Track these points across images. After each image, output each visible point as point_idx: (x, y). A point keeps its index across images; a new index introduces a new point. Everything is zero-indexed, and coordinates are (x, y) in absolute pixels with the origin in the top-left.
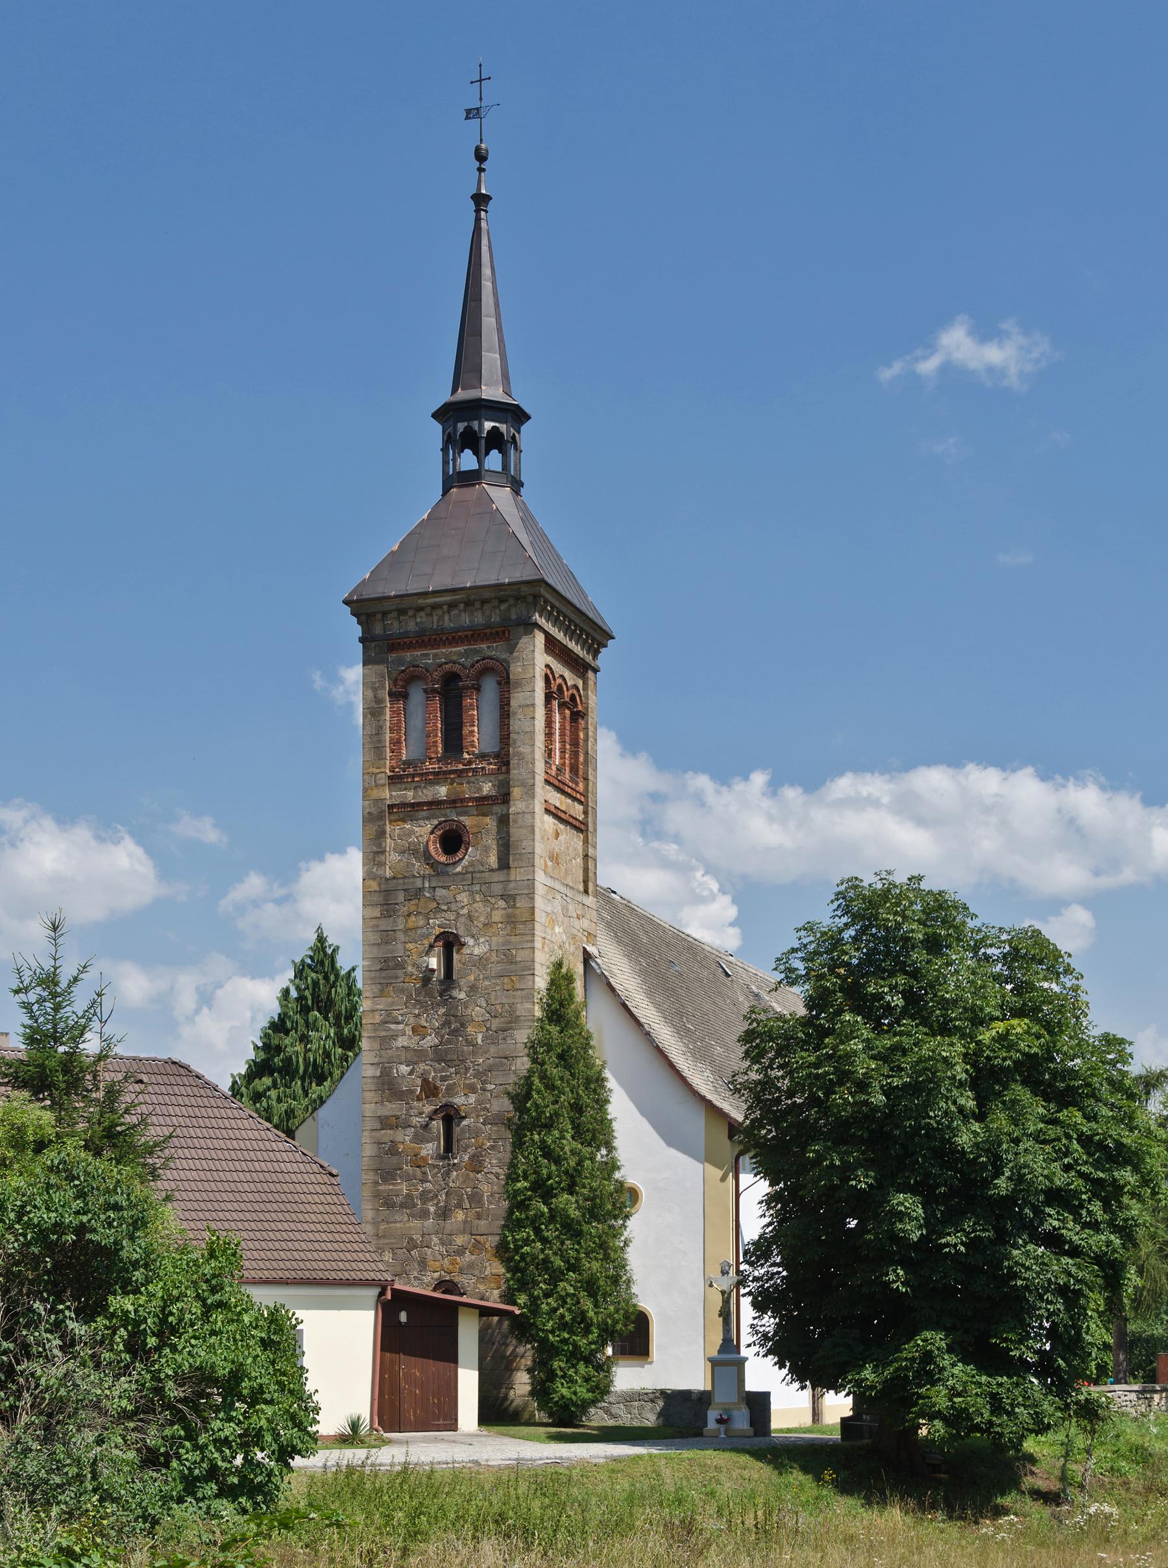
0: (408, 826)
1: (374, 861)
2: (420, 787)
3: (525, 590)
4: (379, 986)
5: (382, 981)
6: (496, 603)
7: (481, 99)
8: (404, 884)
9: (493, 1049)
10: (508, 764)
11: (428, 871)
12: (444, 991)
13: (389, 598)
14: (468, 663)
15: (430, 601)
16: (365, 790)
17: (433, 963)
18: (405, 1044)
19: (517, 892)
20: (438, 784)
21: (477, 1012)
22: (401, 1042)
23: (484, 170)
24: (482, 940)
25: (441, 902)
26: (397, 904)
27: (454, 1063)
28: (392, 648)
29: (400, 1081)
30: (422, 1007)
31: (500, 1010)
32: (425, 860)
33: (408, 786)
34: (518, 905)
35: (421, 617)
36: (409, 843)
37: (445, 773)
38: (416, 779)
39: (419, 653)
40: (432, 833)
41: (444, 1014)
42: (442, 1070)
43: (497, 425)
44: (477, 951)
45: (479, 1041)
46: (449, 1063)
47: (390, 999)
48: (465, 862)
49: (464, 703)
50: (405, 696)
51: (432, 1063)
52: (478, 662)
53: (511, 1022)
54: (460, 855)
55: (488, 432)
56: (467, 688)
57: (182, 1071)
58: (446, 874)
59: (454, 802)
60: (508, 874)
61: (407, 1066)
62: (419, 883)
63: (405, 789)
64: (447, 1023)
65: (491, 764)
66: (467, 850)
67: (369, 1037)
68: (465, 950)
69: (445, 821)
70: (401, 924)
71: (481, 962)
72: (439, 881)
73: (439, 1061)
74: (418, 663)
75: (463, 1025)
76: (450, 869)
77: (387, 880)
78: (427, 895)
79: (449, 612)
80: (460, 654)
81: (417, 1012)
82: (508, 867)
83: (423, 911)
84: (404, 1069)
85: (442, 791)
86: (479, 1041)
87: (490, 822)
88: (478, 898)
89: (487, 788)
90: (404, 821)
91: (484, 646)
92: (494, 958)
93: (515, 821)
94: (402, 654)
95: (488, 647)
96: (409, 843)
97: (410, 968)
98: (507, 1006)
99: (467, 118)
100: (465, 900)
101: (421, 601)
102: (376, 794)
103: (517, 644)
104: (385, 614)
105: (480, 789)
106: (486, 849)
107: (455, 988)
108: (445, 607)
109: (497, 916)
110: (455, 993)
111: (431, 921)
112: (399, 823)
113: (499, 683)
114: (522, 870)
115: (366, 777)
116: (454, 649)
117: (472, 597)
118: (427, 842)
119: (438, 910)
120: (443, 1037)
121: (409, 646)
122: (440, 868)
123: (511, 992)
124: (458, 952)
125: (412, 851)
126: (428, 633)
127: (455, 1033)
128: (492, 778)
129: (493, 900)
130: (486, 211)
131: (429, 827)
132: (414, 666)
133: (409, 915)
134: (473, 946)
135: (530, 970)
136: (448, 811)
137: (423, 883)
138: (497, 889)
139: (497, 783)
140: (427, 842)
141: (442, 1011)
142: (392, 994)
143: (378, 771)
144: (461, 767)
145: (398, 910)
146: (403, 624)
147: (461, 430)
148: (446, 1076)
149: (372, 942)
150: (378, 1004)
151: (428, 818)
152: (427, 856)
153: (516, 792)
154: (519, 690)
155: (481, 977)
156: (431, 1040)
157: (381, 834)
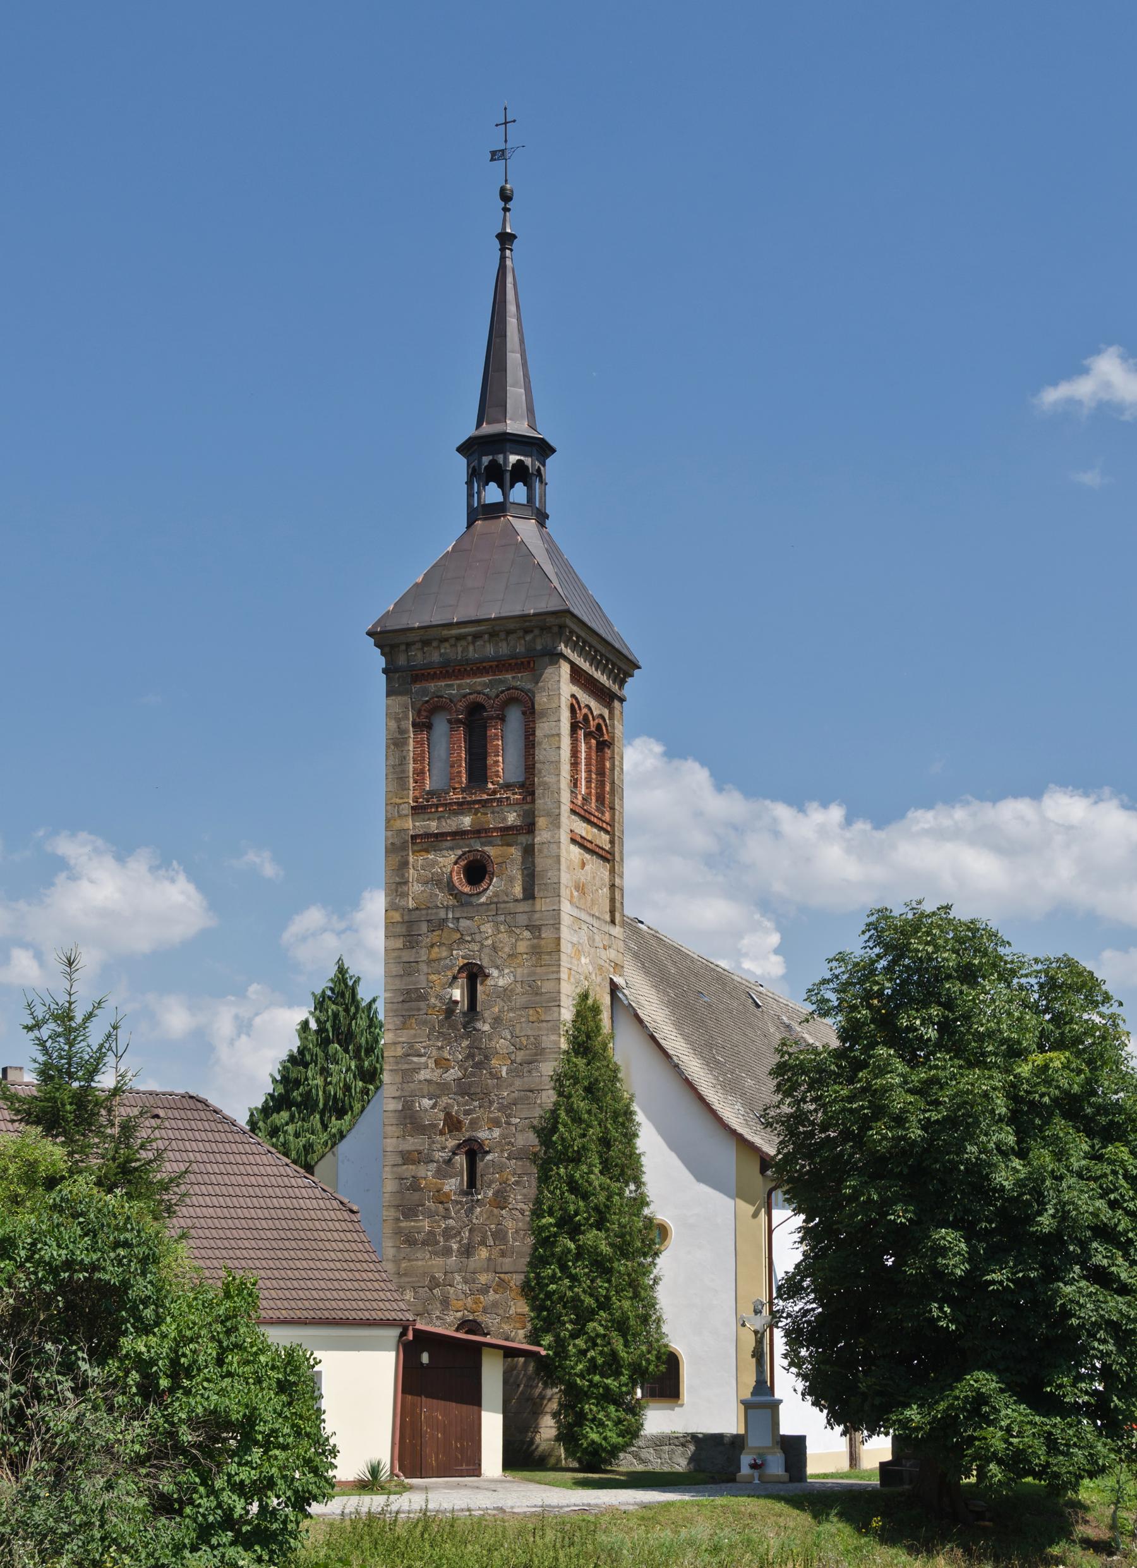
0: (431, 857)
1: (397, 892)
2: (443, 817)
3: (551, 620)
4: (401, 1019)
5: (404, 1013)
6: (521, 633)
8: (427, 915)
9: (518, 1082)
10: (533, 793)
13: (413, 629)
15: (455, 632)
16: (388, 820)
17: (457, 994)
18: (428, 1077)
19: (542, 922)
20: (462, 814)
21: (502, 1044)
22: (424, 1075)
23: (509, 210)
24: (506, 971)
25: (465, 933)
26: (420, 935)
28: (416, 679)
31: (525, 1043)
32: (449, 891)
33: (431, 816)
34: (543, 936)
35: (445, 648)
37: (469, 803)
39: (443, 684)
40: (456, 863)
41: (468, 1047)
42: (466, 1104)
43: (522, 458)
44: (501, 982)
45: (504, 1074)
46: (472, 1096)
47: (412, 1032)
48: (489, 893)
49: (489, 733)
50: (428, 727)
51: (455, 1097)
52: (502, 692)
54: (484, 885)
55: (513, 465)
56: (492, 718)
59: (478, 832)
60: (533, 904)
62: (442, 914)
63: (429, 819)
64: (470, 1056)
65: (516, 793)
66: (491, 880)
67: (391, 1070)
68: (490, 982)
69: (469, 852)
70: (423, 955)
73: (462, 1095)
75: (487, 1057)
76: (474, 900)
78: (451, 925)
80: (485, 685)
81: (440, 1044)
84: (427, 1103)
86: (504, 1074)
87: (515, 852)
88: (502, 928)
89: (512, 818)
90: (427, 851)
91: (509, 676)
92: (519, 989)
93: (540, 851)
95: (513, 678)
97: (433, 1000)
99: (492, 160)
100: (490, 931)
101: (445, 633)
102: (398, 824)
103: (541, 675)
104: (408, 645)
105: (505, 819)
106: (511, 879)
107: (479, 1020)
108: (470, 638)
109: (522, 947)
110: (479, 1025)
111: (455, 952)
112: (423, 853)
113: (524, 713)
116: (479, 680)
117: (497, 628)
120: (466, 1070)
121: (434, 677)
123: (536, 1024)
124: (482, 984)
125: (435, 881)
127: (478, 1066)
128: (517, 808)
129: (518, 931)
130: (511, 250)
131: (453, 858)
132: (437, 697)
133: (432, 946)
134: (498, 977)
135: (556, 1001)
136: (472, 841)
138: (522, 919)
139: (522, 813)
141: (465, 1043)
143: (401, 801)
144: (485, 797)
145: (421, 942)
147: (486, 464)
148: (470, 1110)
151: (452, 849)
152: (451, 887)
153: (541, 822)
154: (544, 720)
155: (506, 1008)
156: (454, 1073)
157: (404, 864)
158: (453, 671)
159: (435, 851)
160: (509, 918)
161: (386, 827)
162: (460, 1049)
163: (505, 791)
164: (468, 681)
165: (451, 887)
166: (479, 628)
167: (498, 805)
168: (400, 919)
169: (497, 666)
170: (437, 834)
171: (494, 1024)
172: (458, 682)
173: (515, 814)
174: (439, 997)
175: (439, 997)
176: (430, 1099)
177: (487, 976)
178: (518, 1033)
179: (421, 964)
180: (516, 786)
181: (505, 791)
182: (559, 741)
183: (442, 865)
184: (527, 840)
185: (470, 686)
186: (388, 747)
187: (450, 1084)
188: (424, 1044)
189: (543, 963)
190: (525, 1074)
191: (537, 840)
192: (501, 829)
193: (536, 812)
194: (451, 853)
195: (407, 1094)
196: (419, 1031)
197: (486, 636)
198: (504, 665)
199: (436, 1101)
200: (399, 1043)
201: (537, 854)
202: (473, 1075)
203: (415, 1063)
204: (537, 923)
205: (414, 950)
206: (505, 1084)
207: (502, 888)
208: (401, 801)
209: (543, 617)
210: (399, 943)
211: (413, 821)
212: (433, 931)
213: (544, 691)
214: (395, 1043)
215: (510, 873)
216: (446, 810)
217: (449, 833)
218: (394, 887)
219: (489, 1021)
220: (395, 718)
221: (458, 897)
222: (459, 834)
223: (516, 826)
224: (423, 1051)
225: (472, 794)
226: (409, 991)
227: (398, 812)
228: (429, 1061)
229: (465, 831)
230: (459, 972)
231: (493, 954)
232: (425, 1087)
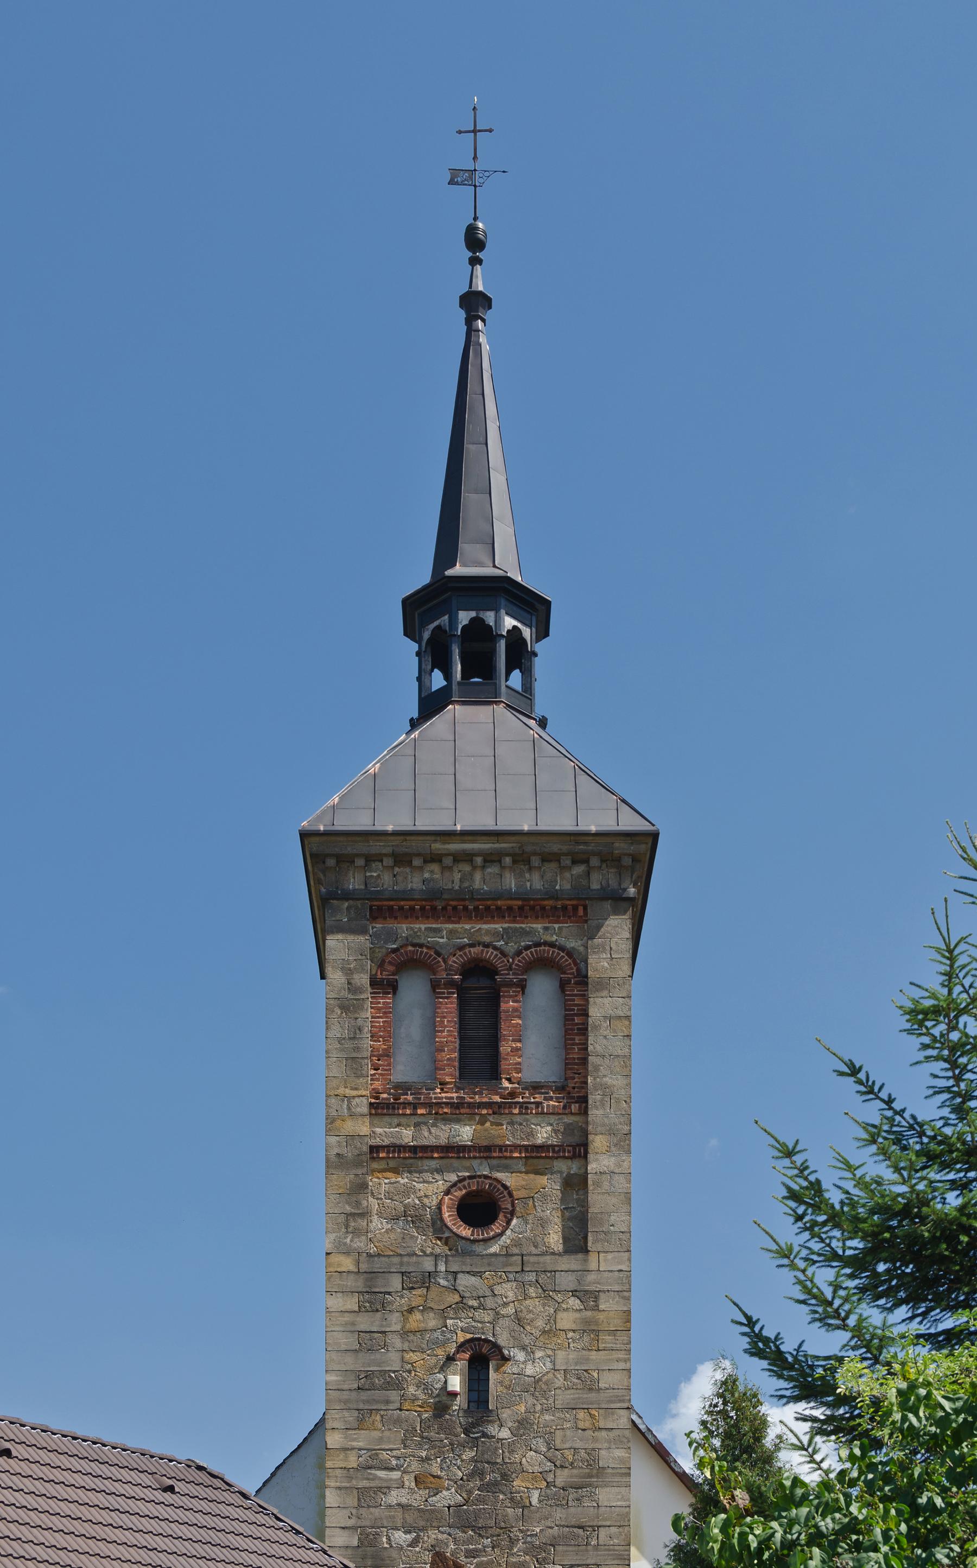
0: (403, 1180)
1: (347, 1227)
2: (425, 1124)
3: (620, 846)
4: (356, 1413)
5: (361, 1406)
6: (567, 861)
7: (475, 158)
8: (401, 1264)
9: (559, 1514)
10: (584, 1100)
11: (440, 1248)
12: (473, 1425)
13: (384, 834)
14: (511, 948)
15: (454, 847)
16: (330, 1120)
17: (455, 1382)
18: (404, 1501)
19: (599, 1287)
20: (458, 1121)
21: (532, 1460)
22: (394, 1497)
23: (480, 262)
24: (539, 1354)
25: (467, 1294)
26: (389, 1293)
27: (490, 1531)
28: (377, 913)
29: (394, 1554)
30: (433, 1447)
31: (570, 1458)
32: (435, 1232)
33: (403, 1120)
34: (602, 1307)
35: (432, 872)
36: (405, 1206)
37: (471, 1105)
38: (420, 1111)
39: (423, 927)
40: (447, 1192)
41: (473, 1460)
42: (470, 1541)
43: (519, 625)
44: (530, 1370)
45: (535, 1501)
46: (480, 1531)
47: (376, 1434)
48: (505, 1240)
49: (503, 1006)
50: (392, 987)
51: (452, 1531)
52: (527, 948)
53: (590, 1476)
54: (496, 1228)
55: (508, 631)
56: (510, 984)
57: (217, 1483)
58: (471, 1254)
59: (488, 1149)
60: (586, 1261)
61: (406, 1532)
62: (428, 1265)
63: (399, 1125)
64: (477, 1473)
65: (551, 1098)
66: (509, 1222)
67: (339, 1488)
68: (509, 1368)
69: (470, 1177)
70: (395, 1322)
71: (537, 1386)
72: (464, 1263)
73: (463, 1528)
74: (422, 941)
75: (505, 1476)
76: (479, 1248)
77: (369, 1255)
78: (443, 1282)
79: (483, 867)
80: (495, 934)
81: (424, 1454)
82: (585, 1251)
83: (435, 1307)
84: (401, 1537)
85: (466, 1133)
86: (535, 1501)
87: (550, 1185)
88: (532, 1291)
89: (543, 1134)
90: (396, 1171)
91: (538, 926)
92: (560, 1381)
93: (598, 1184)
94: (392, 925)
95: (546, 929)
96: (405, 1206)
97: (412, 1390)
98: (582, 1452)
99: (451, 182)
100: (511, 1294)
101: (437, 846)
102: (350, 1127)
103: (599, 927)
104: (370, 859)
105: (532, 1134)
106: (543, 1223)
107: (492, 1422)
108: (479, 860)
109: (566, 1320)
110: (492, 1429)
111: (449, 1322)
112: (389, 1174)
113: (563, 985)
114: (610, 1256)
115: (333, 1101)
116: (485, 926)
117: (529, 849)
118: (439, 1207)
119: (462, 1304)
120: (470, 1492)
121: (410, 914)
122: (461, 1245)
123: (590, 1433)
124: (497, 1370)
125: (412, 1217)
126: (445, 896)
127: (492, 1487)
128: (552, 1119)
129: (559, 1297)
130: (484, 321)
131: (441, 1185)
132: (414, 945)
133: (411, 1310)
134: (525, 1362)
135: (623, 1401)
136: (475, 1163)
137: (436, 1265)
138: (567, 1281)
139: (562, 1128)
140: (439, 1207)
141: (468, 1454)
142: (380, 1426)
143: (354, 1093)
144: (497, 1099)
145: (391, 1303)
146: (400, 878)
147: (465, 622)
148: (476, 1550)
149: (343, 1347)
150: (354, 1440)
151: (439, 1171)
152: (438, 1226)
153: (598, 1142)
154: (605, 993)
155: (538, 1408)
156: (448, 1497)
157: (361, 1187)
158: (444, 908)
159: (410, 1172)
160: (543, 1278)
161: (327, 1131)
162: (459, 1462)
163: (531, 1094)
164: (467, 927)
165: (438, 1226)
166: (497, 845)
167: (520, 1113)
168: (352, 1268)
169: (521, 908)
170: (415, 1147)
171: (518, 1428)
172: (450, 926)
173: (549, 1128)
174: (424, 1386)
175: (424, 1386)
176: (407, 1532)
177: (506, 1359)
178: (558, 1444)
179: (390, 1336)
180: (550, 1087)
181: (531, 1094)
182: (629, 1026)
183: (422, 1193)
184: (570, 1168)
185: (470, 934)
186: (329, 1010)
187: (442, 1511)
188: (395, 1453)
189: (601, 1346)
190: (570, 1503)
191: (592, 1167)
192: (526, 1148)
193: (590, 1128)
194: (437, 1177)
195: (368, 1523)
196: (387, 1433)
197: (508, 860)
198: (532, 908)
199: (418, 1536)
200: (353, 1449)
201: (591, 1188)
202: (480, 1500)
203: (380, 1479)
204: (592, 1288)
205: (379, 1315)
206: (538, 1515)
207: (528, 1234)
208: (354, 1093)
209: (608, 840)
210: (352, 1303)
211: (372, 1125)
212: (413, 1288)
213: (604, 951)
214: (345, 1449)
215: (540, 1214)
216: (430, 1114)
217: (437, 1147)
218: (342, 1218)
219: (510, 1424)
220: (342, 969)
221: (451, 1242)
222: (452, 1151)
223: (553, 1146)
224: (394, 1462)
225: (475, 1093)
226: (369, 1375)
227: (349, 1109)
228: (406, 1477)
229: (465, 1146)
230: (457, 1352)
231: (517, 1328)
232: (399, 1514)
